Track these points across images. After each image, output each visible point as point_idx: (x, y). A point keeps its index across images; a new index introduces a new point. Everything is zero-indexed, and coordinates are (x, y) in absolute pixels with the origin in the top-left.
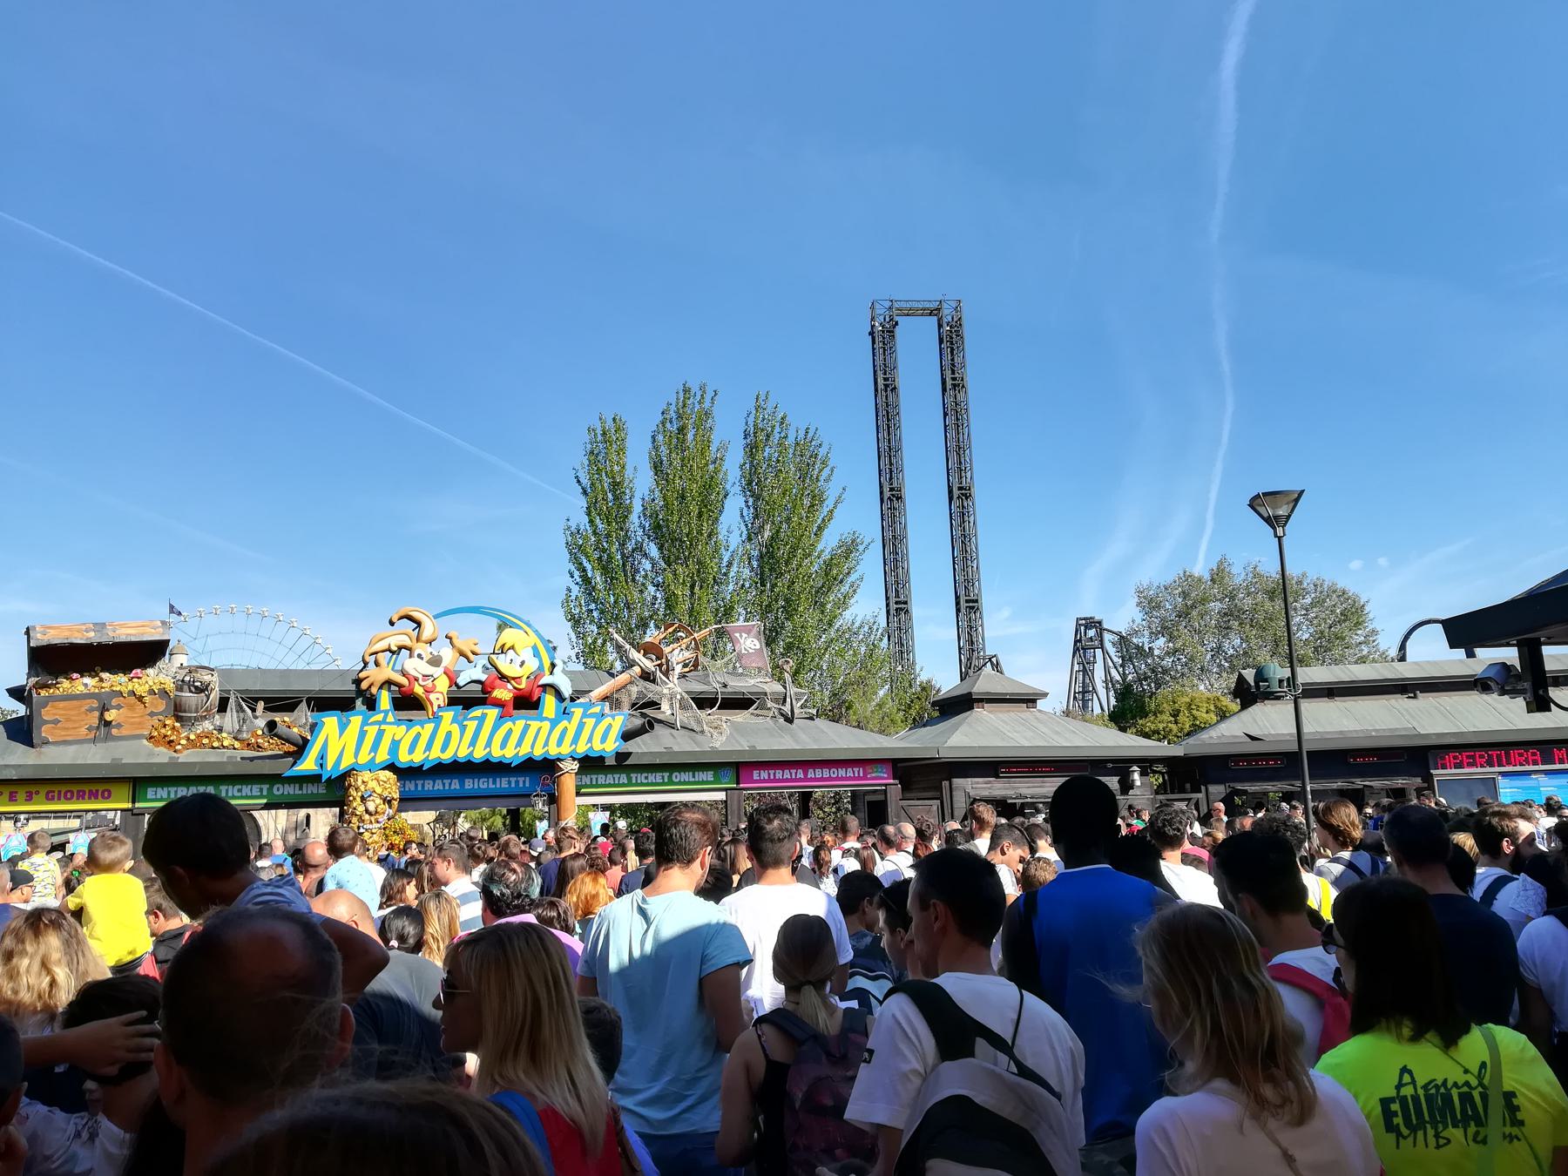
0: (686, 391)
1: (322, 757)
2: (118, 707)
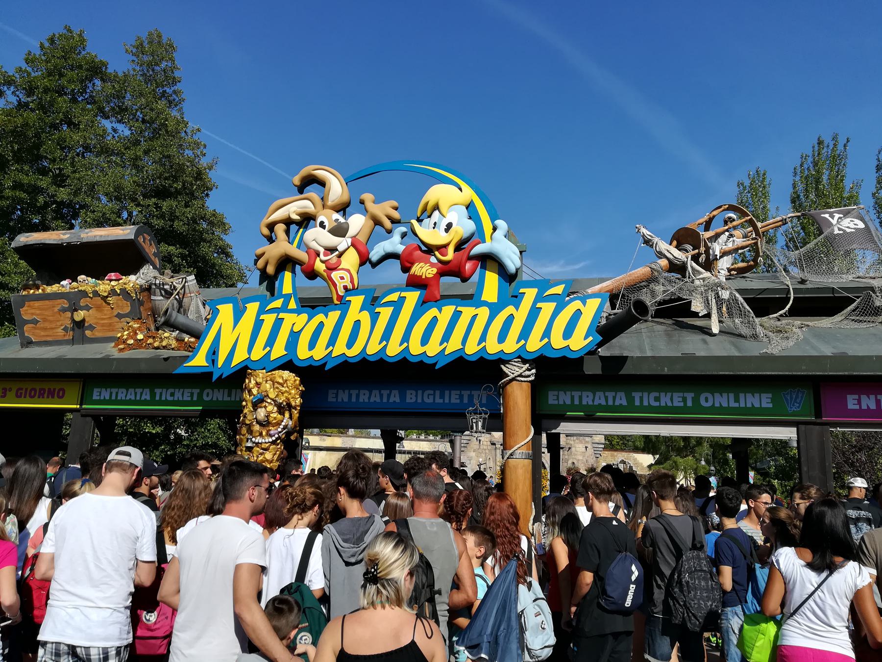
0: (820, 143)
1: (213, 352)
2: (87, 308)
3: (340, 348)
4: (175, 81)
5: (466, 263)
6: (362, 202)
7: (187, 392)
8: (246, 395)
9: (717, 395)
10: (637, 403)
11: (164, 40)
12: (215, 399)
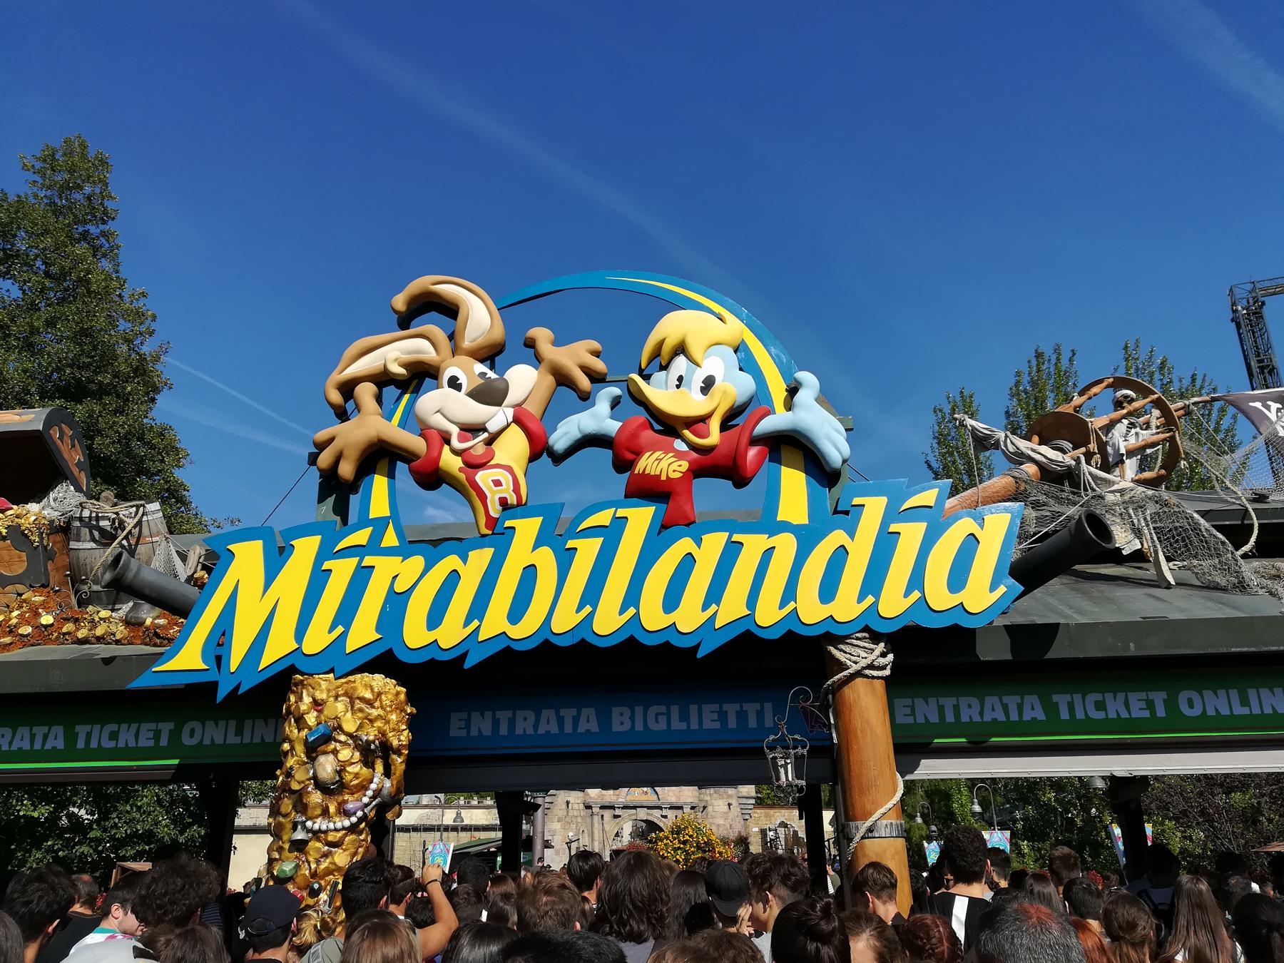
0: (1039, 355)
3: (495, 623)
4: (106, 217)
5: (742, 455)
6: (530, 344)
7: (147, 729)
8: (291, 730)
9: (1208, 694)
10: (1065, 715)
11: (91, 153)
12: (207, 741)
